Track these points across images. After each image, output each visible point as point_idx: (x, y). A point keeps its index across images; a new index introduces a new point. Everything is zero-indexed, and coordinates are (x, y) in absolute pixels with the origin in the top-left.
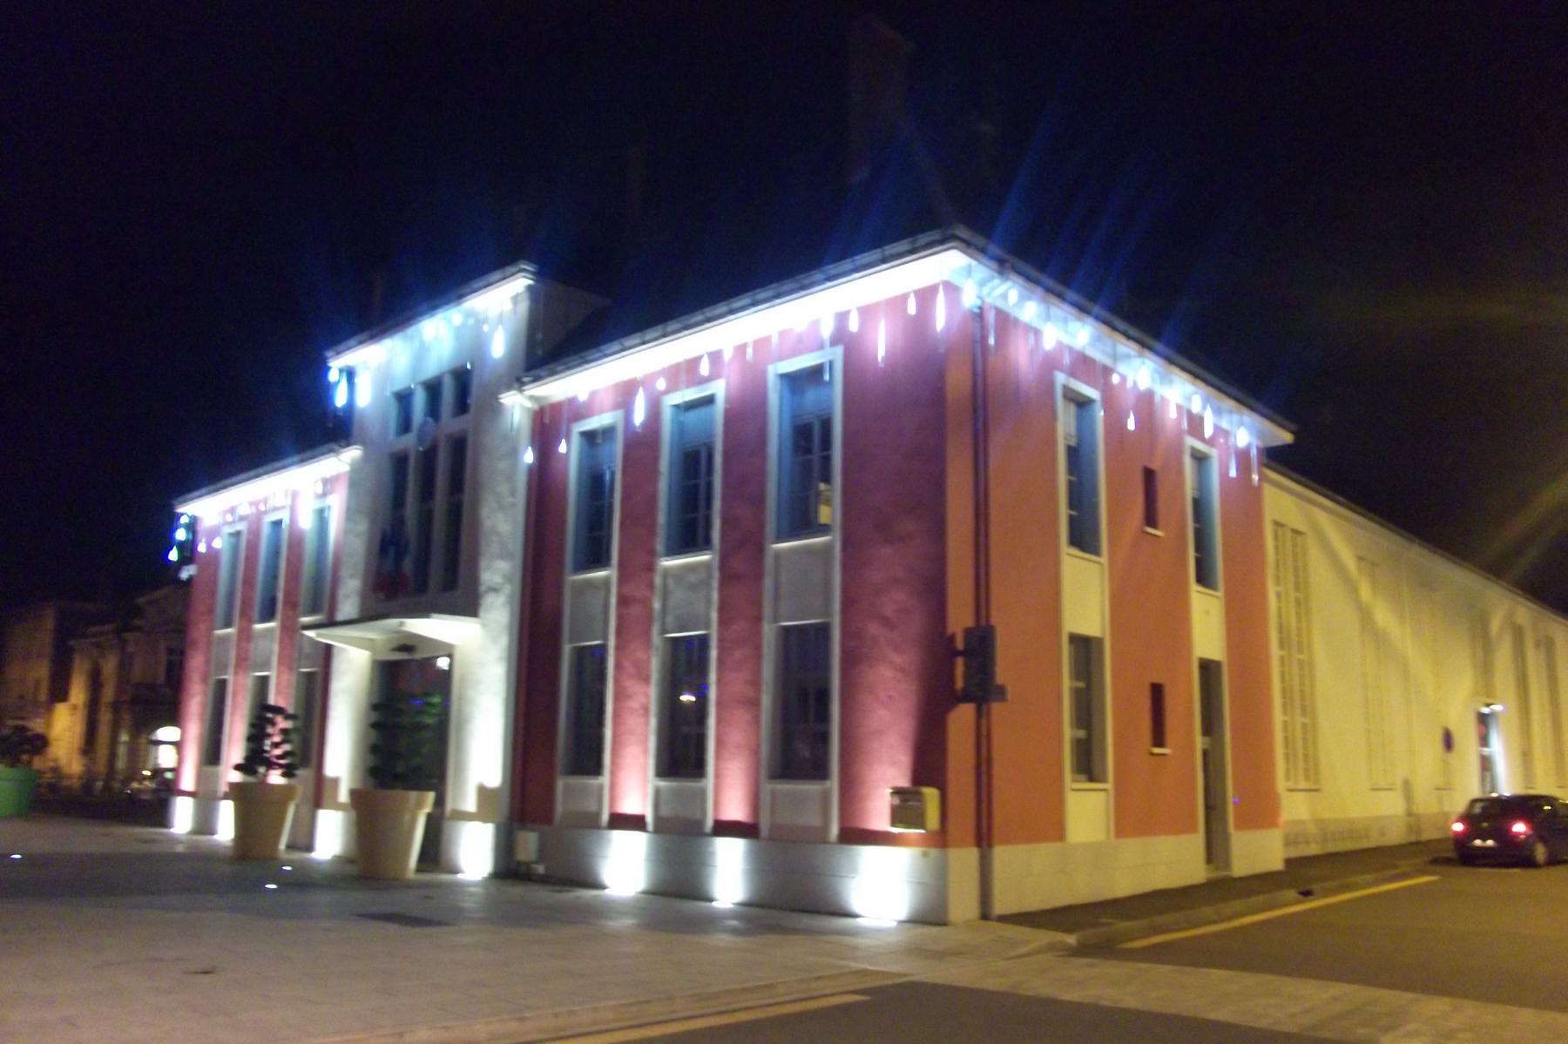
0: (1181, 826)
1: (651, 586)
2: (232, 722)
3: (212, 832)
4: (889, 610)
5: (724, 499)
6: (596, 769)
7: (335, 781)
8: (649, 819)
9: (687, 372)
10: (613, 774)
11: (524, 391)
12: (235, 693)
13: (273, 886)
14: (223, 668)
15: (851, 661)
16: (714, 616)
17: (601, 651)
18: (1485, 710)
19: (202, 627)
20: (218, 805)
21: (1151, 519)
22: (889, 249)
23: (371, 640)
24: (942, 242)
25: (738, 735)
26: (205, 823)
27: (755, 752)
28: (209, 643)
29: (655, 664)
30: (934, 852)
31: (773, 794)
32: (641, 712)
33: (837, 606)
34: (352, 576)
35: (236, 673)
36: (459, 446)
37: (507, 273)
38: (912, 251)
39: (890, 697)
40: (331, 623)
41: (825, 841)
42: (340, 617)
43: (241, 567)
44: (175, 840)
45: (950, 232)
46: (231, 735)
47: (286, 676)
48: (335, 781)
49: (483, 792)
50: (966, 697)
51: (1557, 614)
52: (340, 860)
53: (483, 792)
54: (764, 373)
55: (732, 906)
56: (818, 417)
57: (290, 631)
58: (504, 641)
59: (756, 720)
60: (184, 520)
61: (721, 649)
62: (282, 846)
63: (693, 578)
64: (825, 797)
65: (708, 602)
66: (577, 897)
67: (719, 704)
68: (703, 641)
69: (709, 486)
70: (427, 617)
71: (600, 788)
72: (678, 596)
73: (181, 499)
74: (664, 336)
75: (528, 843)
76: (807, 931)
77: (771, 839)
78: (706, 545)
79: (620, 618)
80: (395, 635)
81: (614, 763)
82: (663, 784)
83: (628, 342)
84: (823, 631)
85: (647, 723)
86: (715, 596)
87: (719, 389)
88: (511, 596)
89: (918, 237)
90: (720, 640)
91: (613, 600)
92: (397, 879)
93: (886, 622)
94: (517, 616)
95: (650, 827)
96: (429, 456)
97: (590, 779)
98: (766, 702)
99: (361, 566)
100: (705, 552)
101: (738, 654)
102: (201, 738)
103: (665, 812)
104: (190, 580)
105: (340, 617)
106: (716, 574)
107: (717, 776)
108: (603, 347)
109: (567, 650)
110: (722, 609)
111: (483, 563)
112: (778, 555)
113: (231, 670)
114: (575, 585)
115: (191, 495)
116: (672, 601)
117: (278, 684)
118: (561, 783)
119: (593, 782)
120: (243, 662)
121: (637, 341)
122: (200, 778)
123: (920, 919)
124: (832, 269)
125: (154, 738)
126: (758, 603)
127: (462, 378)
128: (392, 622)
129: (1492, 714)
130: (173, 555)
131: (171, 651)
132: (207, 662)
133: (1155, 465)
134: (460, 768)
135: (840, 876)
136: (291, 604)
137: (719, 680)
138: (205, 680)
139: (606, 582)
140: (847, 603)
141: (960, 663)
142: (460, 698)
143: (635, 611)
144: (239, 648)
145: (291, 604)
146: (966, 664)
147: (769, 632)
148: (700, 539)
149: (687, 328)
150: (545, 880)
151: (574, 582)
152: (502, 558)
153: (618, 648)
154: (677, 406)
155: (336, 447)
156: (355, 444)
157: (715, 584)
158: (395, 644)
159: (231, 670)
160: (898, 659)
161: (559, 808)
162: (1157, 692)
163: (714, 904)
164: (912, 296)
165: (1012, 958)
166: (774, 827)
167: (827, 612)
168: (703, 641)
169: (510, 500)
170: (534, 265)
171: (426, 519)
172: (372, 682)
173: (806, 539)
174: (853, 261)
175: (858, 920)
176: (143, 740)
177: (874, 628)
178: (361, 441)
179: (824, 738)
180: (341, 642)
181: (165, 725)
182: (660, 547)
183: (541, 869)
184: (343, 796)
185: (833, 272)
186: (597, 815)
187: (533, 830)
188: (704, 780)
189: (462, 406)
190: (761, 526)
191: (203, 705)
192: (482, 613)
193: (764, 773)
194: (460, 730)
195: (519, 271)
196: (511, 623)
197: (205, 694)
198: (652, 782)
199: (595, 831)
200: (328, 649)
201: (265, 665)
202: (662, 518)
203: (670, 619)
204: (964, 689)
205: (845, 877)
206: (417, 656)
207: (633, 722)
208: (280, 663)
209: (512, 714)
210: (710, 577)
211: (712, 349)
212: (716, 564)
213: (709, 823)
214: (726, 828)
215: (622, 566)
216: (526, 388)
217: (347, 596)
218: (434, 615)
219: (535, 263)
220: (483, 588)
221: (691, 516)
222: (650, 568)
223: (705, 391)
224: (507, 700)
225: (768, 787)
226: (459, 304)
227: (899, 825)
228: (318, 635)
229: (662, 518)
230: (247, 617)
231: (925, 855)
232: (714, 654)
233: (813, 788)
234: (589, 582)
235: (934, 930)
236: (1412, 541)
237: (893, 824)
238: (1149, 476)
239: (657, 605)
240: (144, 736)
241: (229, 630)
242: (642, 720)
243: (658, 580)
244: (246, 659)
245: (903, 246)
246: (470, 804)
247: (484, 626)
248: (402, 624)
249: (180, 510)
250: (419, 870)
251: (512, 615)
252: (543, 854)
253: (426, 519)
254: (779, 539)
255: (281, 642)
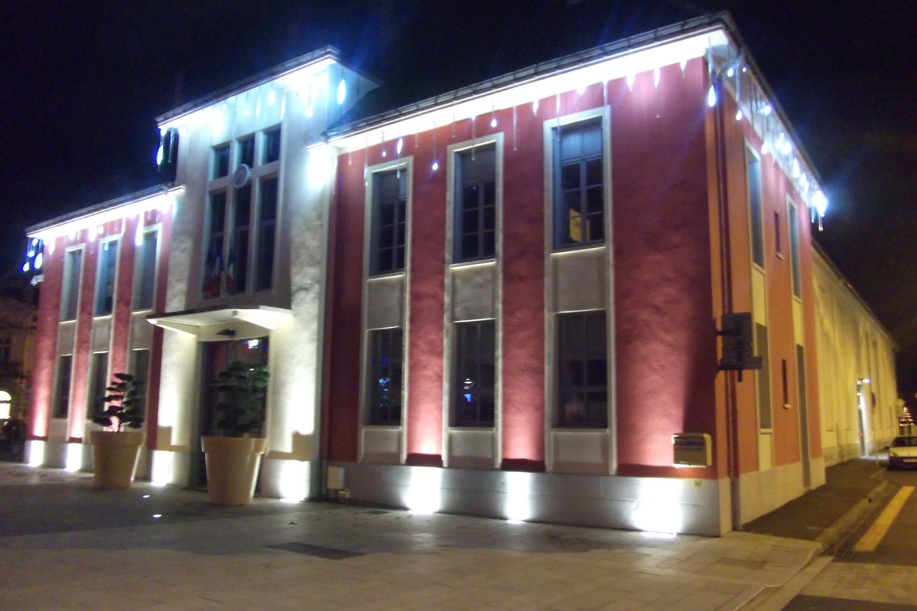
0: (794, 461)
1: (442, 285)
2: (75, 389)
4: (659, 301)
7: (169, 430)
8: (444, 458)
11: (330, 142)
14: (70, 349)
15: (624, 339)
16: (500, 307)
17: (399, 333)
23: (198, 326)
24: (710, 24)
25: (523, 394)
26: (55, 459)
27: (540, 408)
29: (447, 343)
30: (705, 482)
31: (557, 440)
32: (435, 378)
33: (612, 299)
35: (78, 352)
36: (270, 185)
38: (683, 32)
39: (662, 366)
41: (607, 474)
42: (168, 310)
44: (30, 473)
46: (74, 396)
47: (121, 354)
48: (169, 430)
50: (725, 367)
51: (882, 328)
53: (297, 437)
54: (63, 252)
56: (584, 160)
57: (123, 321)
58: (314, 326)
60: (34, 243)
61: (506, 333)
62: (132, 479)
63: (479, 280)
65: (494, 297)
66: (387, 517)
67: (505, 372)
68: (490, 327)
70: (257, 308)
71: (400, 435)
72: (465, 293)
73: (33, 227)
75: (337, 476)
76: (601, 545)
77: (554, 472)
78: (489, 253)
79: (413, 309)
82: (455, 432)
84: (601, 316)
85: (441, 387)
86: (500, 292)
87: (499, 139)
88: (319, 293)
91: (408, 296)
92: (242, 505)
93: (657, 310)
95: (445, 464)
98: (548, 370)
99: (186, 274)
100: (397, 273)
102: (50, 400)
103: (458, 452)
104: (39, 284)
105: (168, 310)
106: (500, 276)
107: (505, 425)
109: (366, 333)
110: (505, 302)
111: (294, 270)
112: (556, 261)
113: (75, 350)
115: (39, 225)
116: (460, 297)
117: (114, 360)
118: (364, 432)
119: (394, 430)
120: (84, 344)
122: (49, 428)
123: (694, 532)
124: (609, 46)
126: (540, 297)
127: (274, 134)
128: (228, 312)
130: (26, 268)
132: (54, 345)
134: (278, 421)
136: (125, 301)
137: (505, 355)
138: (52, 357)
139: (401, 283)
140: (620, 296)
141: (719, 339)
143: (425, 304)
144: (80, 332)
146: (724, 341)
147: (549, 318)
148: (394, 264)
150: (352, 503)
151: (552, 256)
153: (411, 332)
154: (554, 129)
155: (164, 187)
157: (500, 282)
158: (219, 330)
159: (75, 350)
160: (669, 338)
161: (362, 450)
163: (282, 501)
165: (809, 564)
166: (557, 463)
167: (603, 300)
168: (490, 327)
170: (339, 50)
171: (242, 239)
174: (628, 40)
175: (642, 533)
179: (603, 397)
180: (173, 327)
181: (7, 392)
182: (448, 256)
183: (347, 494)
184: (175, 439)
185: (497, 82)
187: (339, 466)
189: (273, 154)
191: (52, 374)
192: (293, 306)
193: (547, 425)
196: (319, 314)
197: (53, 367)
198: (446, 430)
199: (395, 467)
200: (159, 333)
202: (449, 234)
203: (458, 309)
204: (722, 360)
205: (499, 492)
206: (236, 338)
207: (427, 386)
208: (115, 344)
209: (320, 381)
210: (495, 278)
212: (500, 268)
213: (499, 460)
215: (413, 270)
217: (174, 296)
218: (261, 307)
220: (294, 288)
222: (441, 272)
224: (317, 369)
225: (551, 435)
227: (683, 462)
228: (159, 322)
229: (449, 234)
230: (86, 310)
231: (697, 484)
232: (500, 335)
233: (594, 434)
235: (715, 540)
236: (840, 278)
237: (677, 461)
239: (447, 299)
242: (436, 384)
243: (447, 281)
244: (88, 341)
245: (675, 27)
246: (287, 446)
247: (295, 315)
248: (235, 313)
249: (30, 236)
250: (256, 496)
251: (319, 308)
252: (348, 484)
253: (242, 239)
254: (555, 250)
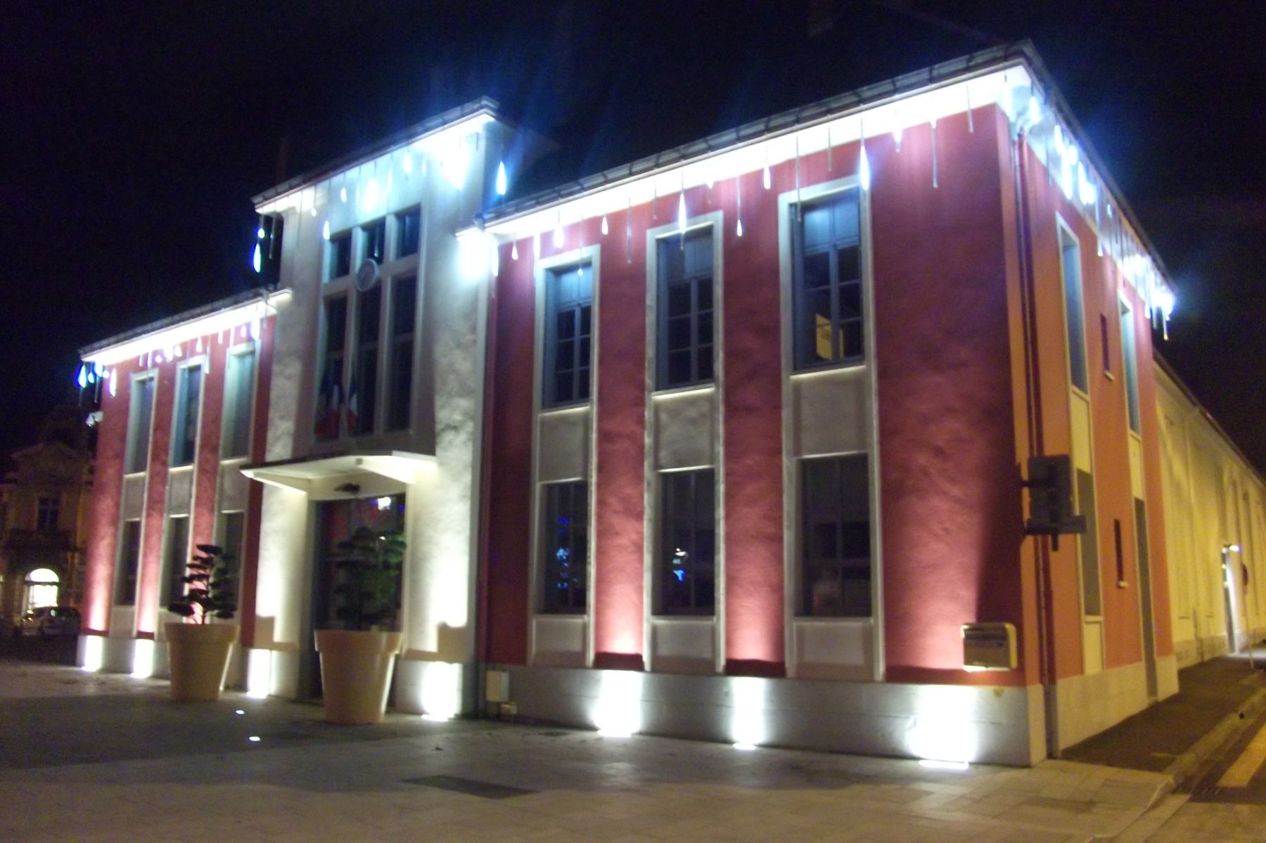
0: (1134, 659)
1: (640, 421)
3: (126, 669)
5: (728, 333)
6: (579, 605)
7: (270, 621)
8: (646, 659)
9: (663, 210)
10: (598, 613)
12: (147, 537)
13: (255, 739)
14: (138, 512)
15: (892, 493)
16: (720, 449)
17: (583, 487)
18: (1224, 550)
19: (111, 472)
20: (134, 644)
21: (1106, 366)
22: (939, 69)
23: (309, 481)
24: (1005, 58)
25: (754, 569)
26: (118, 660)
27: (778, 589)
28: (119, 488)
30: (1009, 691)
31: (801, 634)
32: (632, 548)
34: (282, 418)
36: (406, 288)
37: (466, 110)
38: (968, 69)
39: (946, 530)
40: (259, 462)
42: (270, 457)
43: (1021, 209)
45: (1014, 48)
47: (205, 519)
48: (270, 621)
49: (444, 630)
50: (1033, 530)
52: (274, 701)
53: (444, 630)
55: (753, 748)
57: (209, 472)
58: (467, 478)
59: (778, 558)
62: (221, 688)
63: (692, 412)
64: (868, 639)
69: (586, 345)
70: (390, 454)
72: (672, 431)
74: (658, 166)
75: (498, 684)
77: (799, 678)
78: (706, 375)
80: (340, 475)
81: (598, 601)
82: (661, 622)
83: (611, 174)
84: (861, 462)
86: (721, 429)
88: (473, 433)
89: (975, 54)
90: (728, 474)
91: (594, 436)
92: (370, 724)
93: (939, 452)
94: (479, 454)
95: (647, 666)
96: (370, 299)
97: (573, 618)
98: (789, 536)
101: (750, 489)
103: (664, 651)
106: (722, 408)
107: (729, 613)
108: (581, 180)
109: (538, 487)
110: (728, 444)
111: (439, 401)
112: (798, 387)
114: (544, 423)
116: (665, 436)
117: (196, 526)
118: (534, 623)
119: (577, 621)
121: (626, 172)
125: (27, 579)
127: (410, 218)
129: (1228, 554)
131: (43, 501)
133: (1106, 315)
134: (418, 609)
135: (890, 716)
136: (211, 446)
137: (728, 516)
138: (114, 522)
139: (586, 418)
141: (1026, 492)
142: (415, 536)
143: (621, 446)
145: (211, 446)
146: (1031, 495)
147: (788, 464)
149: (684, 157)
150: (519, 721)
151: (543, 419)
152: (461, 396)
153: (599, 485)
155: (263, 291)
156: (283, 288)
158: (337, 484)
160: (956, 491)
161: (533, 649)
162: (1117, 525)
164: (682, 197)
166: (802, 667)
169: (470, 337)
170: (498, 103)
171: (368, 361)
172: (308, 525)
173: (828, 370)
175: (921, 762)
176: (18, 581)
177: (922, 459)
178: (291, 286)
179: (865, 573)
182: (649, 381)
183: (512, 709)
184: (279, 635)
185: (834, 105)
186: (583, 654)
187: (503, 670)
188: (715, 619)
189: (409, 244)
190: (777, 357)
191: (113, 547)
192: (438, 451)
193: (788, 611)
194: (416, 568)
195: (482, 107)
197: (115, 536)
200: (256, 490)
201: (184, 507)
202: (650, 352)
203: (663, 454)
206: (362, 496)
207: (621, 559)
211: (247, 320)
212: (721, 396)
213: (722, 662)
214: (739, 668)
216: (486, 225)
217: (278, 438)
219: (497, 100)
220: (439, 427)
221: (704, 346)
222: (640, 402)
223: (697, 223)
224: (471, 539)
225: (793, 625)
226: (409, 144)
228: (257, 475)
229: (650, 352)
231: (998, 694)
232: (721, 488)
233: (853, 625)
234: (564, 419)
237: (968, 661)
238: (1103, 320)
239: (648, 440)
240: (19, 577)
241: (141, 474)
243: (648, 415)
244: (161, 501)
245: (959, 63)
246: (430, 643)
247: (441, 464)
248: (360, 462)
250: (388, 712)
251: (474, 452)
252: (513, 694)
253: (368, 361)
255: (199, 484)
